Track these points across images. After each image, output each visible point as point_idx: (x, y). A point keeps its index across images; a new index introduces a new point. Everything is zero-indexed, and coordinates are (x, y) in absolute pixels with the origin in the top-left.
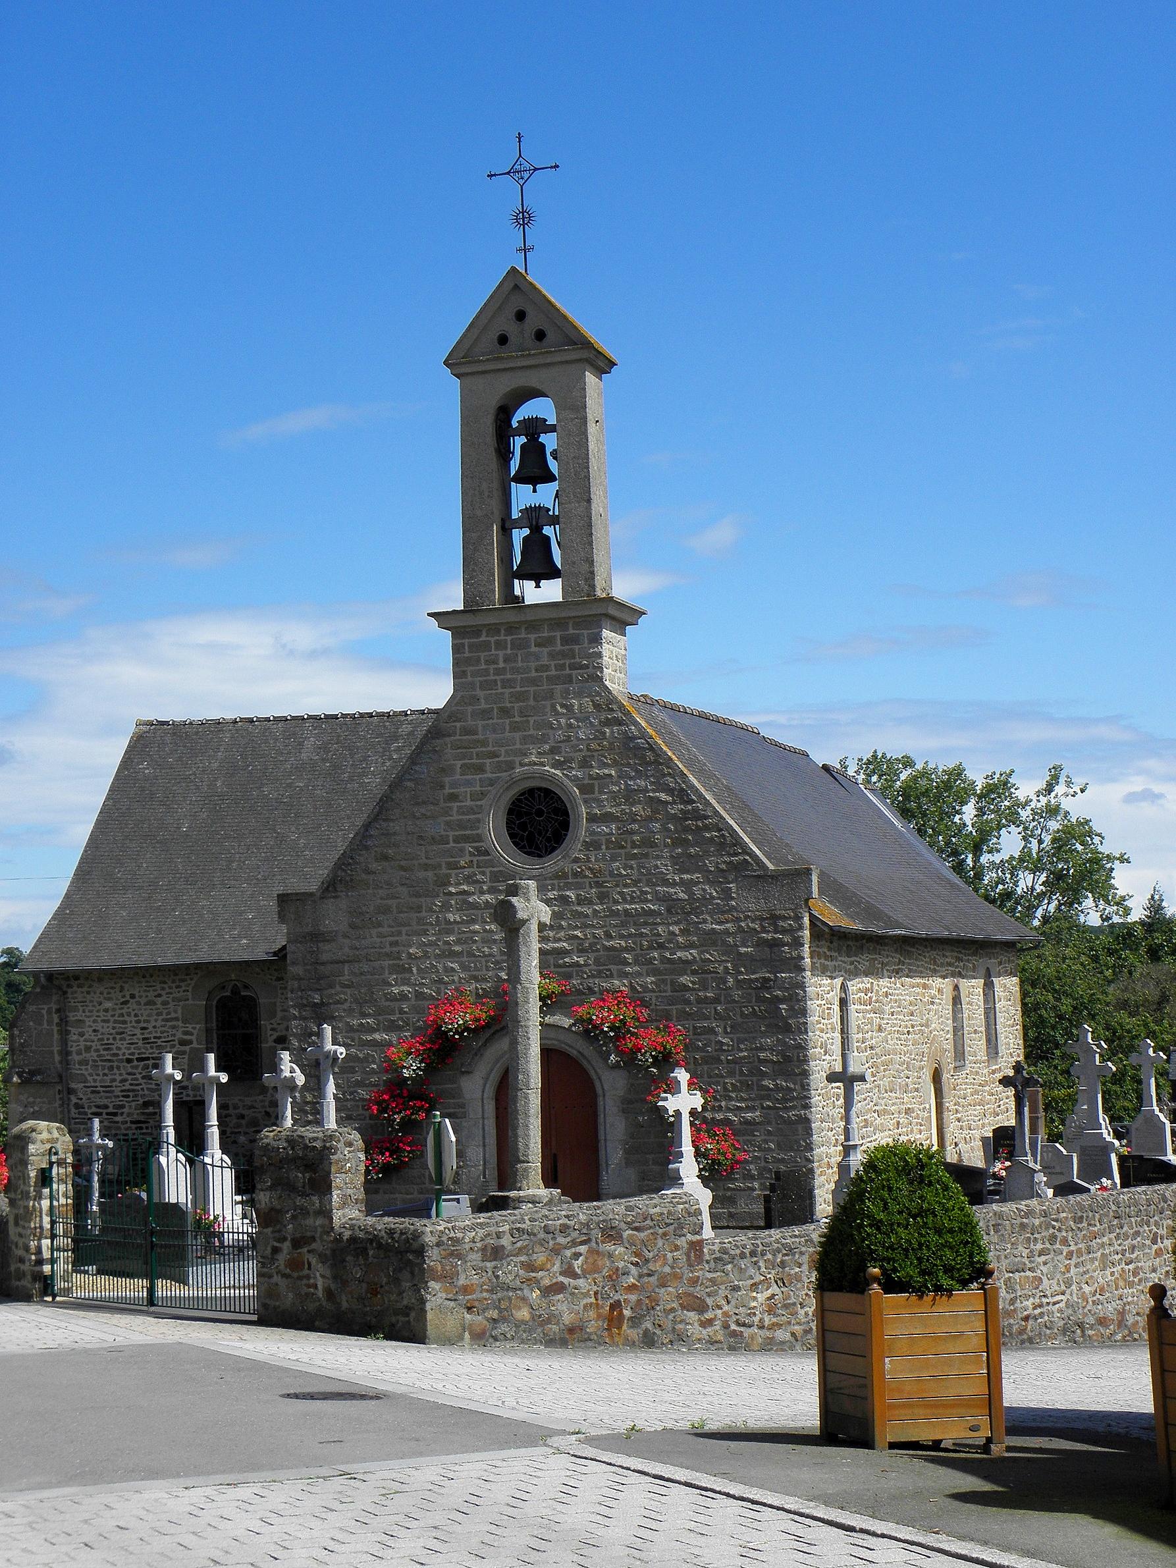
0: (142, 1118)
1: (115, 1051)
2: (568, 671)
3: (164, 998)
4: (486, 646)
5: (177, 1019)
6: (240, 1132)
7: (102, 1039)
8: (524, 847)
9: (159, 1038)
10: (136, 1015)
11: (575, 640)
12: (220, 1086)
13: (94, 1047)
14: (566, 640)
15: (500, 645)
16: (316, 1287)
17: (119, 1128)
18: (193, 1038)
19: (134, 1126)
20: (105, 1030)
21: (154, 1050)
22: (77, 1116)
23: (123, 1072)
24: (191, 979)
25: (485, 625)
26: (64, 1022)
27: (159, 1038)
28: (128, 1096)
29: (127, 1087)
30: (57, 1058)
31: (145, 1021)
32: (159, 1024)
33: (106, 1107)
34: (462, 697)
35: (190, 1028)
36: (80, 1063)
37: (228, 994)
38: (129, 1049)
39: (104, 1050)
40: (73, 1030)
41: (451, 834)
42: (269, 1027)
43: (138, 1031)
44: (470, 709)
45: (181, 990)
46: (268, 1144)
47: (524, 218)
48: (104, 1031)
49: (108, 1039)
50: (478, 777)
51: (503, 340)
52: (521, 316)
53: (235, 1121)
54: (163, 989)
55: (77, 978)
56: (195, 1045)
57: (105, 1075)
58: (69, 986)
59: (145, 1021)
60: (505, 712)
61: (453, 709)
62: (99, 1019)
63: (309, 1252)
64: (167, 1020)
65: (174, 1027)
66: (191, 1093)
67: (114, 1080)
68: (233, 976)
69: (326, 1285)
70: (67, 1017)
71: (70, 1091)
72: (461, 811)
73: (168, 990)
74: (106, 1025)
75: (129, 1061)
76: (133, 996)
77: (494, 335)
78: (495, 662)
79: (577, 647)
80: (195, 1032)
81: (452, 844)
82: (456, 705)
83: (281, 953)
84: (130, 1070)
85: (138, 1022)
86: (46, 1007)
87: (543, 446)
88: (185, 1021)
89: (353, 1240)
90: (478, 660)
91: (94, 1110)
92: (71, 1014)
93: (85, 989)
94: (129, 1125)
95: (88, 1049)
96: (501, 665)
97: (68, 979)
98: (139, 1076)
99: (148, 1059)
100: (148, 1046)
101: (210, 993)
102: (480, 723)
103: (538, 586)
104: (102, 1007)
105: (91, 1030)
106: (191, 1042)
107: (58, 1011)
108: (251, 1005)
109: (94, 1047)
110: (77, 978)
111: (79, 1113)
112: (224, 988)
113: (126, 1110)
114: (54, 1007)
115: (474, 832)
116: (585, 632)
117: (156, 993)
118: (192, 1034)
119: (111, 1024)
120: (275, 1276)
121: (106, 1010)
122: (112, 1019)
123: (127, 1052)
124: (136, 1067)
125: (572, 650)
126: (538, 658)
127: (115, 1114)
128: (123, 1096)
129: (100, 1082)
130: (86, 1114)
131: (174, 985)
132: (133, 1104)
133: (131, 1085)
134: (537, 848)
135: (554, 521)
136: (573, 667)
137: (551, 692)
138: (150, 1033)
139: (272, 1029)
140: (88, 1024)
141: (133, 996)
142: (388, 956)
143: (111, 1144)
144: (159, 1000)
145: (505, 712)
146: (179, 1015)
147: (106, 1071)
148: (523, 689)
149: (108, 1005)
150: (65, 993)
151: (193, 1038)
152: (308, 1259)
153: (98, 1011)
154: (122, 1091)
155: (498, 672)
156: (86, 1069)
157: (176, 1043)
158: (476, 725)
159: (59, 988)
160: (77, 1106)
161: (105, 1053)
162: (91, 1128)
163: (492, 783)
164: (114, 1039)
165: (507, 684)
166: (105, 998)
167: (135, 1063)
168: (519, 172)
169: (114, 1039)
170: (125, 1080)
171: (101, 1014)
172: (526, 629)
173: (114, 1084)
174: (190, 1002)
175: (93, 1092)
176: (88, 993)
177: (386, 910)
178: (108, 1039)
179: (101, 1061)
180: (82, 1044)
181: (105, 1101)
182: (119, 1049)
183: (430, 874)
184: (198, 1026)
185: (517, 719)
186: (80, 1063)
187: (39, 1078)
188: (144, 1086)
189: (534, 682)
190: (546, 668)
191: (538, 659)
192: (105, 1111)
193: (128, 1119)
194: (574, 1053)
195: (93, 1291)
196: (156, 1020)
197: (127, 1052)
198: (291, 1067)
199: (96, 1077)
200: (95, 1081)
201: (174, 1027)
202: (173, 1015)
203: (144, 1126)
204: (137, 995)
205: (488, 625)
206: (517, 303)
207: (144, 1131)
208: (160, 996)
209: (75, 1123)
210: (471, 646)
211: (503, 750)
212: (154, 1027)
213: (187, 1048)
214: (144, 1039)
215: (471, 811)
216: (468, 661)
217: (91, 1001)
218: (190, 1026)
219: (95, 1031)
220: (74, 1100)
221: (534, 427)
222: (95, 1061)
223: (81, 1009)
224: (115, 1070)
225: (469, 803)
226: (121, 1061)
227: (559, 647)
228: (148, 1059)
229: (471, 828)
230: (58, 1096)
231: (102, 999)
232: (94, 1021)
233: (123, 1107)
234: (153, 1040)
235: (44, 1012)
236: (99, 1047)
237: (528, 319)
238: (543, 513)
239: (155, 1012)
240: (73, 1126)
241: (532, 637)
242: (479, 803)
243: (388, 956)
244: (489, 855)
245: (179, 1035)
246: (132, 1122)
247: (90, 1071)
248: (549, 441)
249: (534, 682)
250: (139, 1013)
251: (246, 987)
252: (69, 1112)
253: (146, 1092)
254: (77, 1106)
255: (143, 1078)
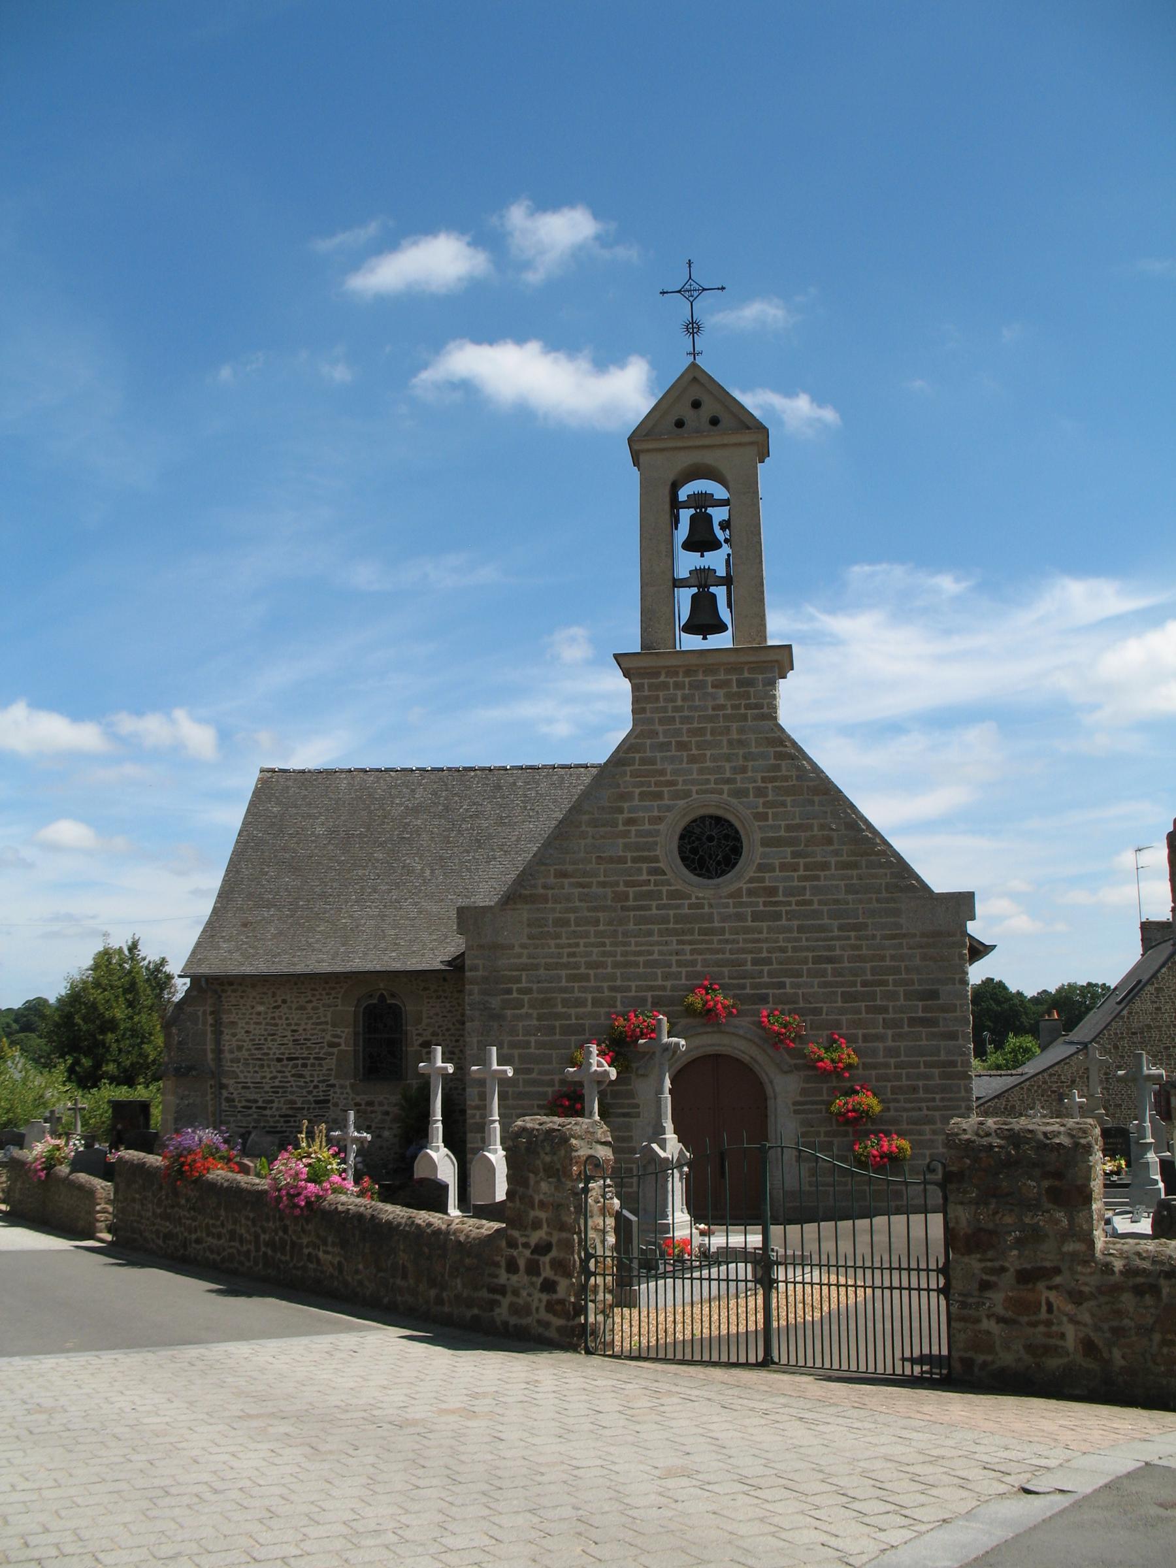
0: (290, 1112)
1: (265, 1051)
2: (743, 711)
3: (314, 1004)
4: (665, 686)
5: (326, 1023)
6: (384, 1128)
7: (254, 1040)
8: (695, 869)
9: (309, 1040)
10: (287, 1019)
11: (750, 683)
12: (504, 1081)
13: (246, 1047)
14: (740, 683)
15: (678, 686)
16: (1063, 1336)
17: (268, 1121)
18: (342, 1041)
19: (282, 1119)
20: (257, 1032)
21: (304, 1051)
22: (227, 1109)
23: (272, 1069)
24: (341, 987)
25: (664, 667)
26: (218, 1025)
27: (309, 1040)
28: (278, 1092)
29: (277, 1084)
30: (210, 1056)
31: (296, 1024)
32: (309, 1027)
33: (256, 1101)
34: (641, 730)
35: (339, 1031)
36: (232, 1061)
37: (375, 1001)
38: (280, 1049)
39: (256, 1049)
40: (226, 1031)
41: (629, 855)
42: (415, 1032)
43: (289, 1033)
44: (648, 742)
45: (331, 997)
46: (969, 1141)
47: (693, 328)
48: (256, 1032)
49: (260, 1040)
50: (655, 804)
51: (680, 424)
52: (696, 405)
53: (379, 1117)
54: (313, 995)
55: (231, 984)
56: (343, 1047)
57: (256, 1072)
58: (223, 991)
59: (296, 1024)
60: (682, 746)
61: (633, 741)
62: (252, 1022)
63: (1049, 1288)
64: (317, 1024)
65: (324, 1030)
66: (338, 1091)
67: (264, 1077)
68: (382, 986)
69: (1081, 1335)
70: (221, 1018)
71: (223, 1086)
72: (639, 834)
73: (318, 997)
74: (258, 1027)
75: (279, 1060)
76: (284, 1001)
77: (672, 419)
78: (673, 700)
79: (752, 690)
80: (344, 1035)
81: (629, 864)
82: (635, 738)
83: (457, 965)
84: (279, 1068)
85: (289, 1025)
86: (202, 1009)
87: (710, 517)
88: (334, 1025)
89: (1130, 1272)
90: (657, 699)
91: (244, 1104)
92: (225, 1016)
93: (239, 994)
94: (277, 1118)
95: (240, 1048)
96: (679, 703)
97: (222, 984)
98: (289, 1074)
99: (297, 1059)
100: (298, 1047)
101: (359, 1000)
102: (659, 755)
103: (705, 638)
104: (254, 1011)
105: (243, 1031)
106: (339, 1045)
107: (212, 1013)
108: (395, 1013)
109: (246, 1047)
110: (231, 984)
111: (230, 1106)
112: (371, 996)
113: (275, 1105)
114: (209, 1009)
115: (651, 854)
116: (760, 677)
117: (307, 999)
118: (340, 1037)
119: (263, 1027)
120: (985, 1321)
121: (259, 1014)
122: (264, 1022)
123: (278, 1052)
124: (286, 1066)
125: (748, 692)
126: (714, 699)
127: (265, 1108)
128: (273, 1092)
129: (251, 1078)
130: (236, 1107)
131: (324, 992)
132: (282, 1100)
133: (281, 1082)
134: (708, 870)
135: (721, 581)
136: (747, 707)
137: (728, 729)
138: (301, 1035)
139: (417, 1035)
140: (240, 1025)
141: (284, 1001)
142: (566, 966)
143: (369, 1137)
144: (310, 1006)
145: (682, 746)
146: (329, 1019)
147: (257, 1069)
148: (701, 726)
149: (261, 1008)
150: (220, 997)
151: (342, 1041)
152: (1047, 1299)
153: (251, 1014)
154: (272, 1087)
155: (676, 709)
156: (238, 1067)
157: (325, 1044)
158: (656, 756)
159: (216, 992)
160: (228, 1100)
161: (256, 1052)
162: (346, 1120)
163: (669, 808)
164: (266, 1040)
165: (686, 720)
166: (258, 1003)
167: (285, 1062)
168: (690, 291)
169: (266, 1040)
170: (275, 1078)
171: (254, 1016)
172: (704, 672)
173: (264, 1081)
174: (339, 1008)
175: (244, 1088)
176: (242, 997)
177: (565, 923)
178: (260, 1040)
179: (253, 1059)
180: (234, 1043)
181: (252, 1097)
182: (270, 1048)
183: (609, 890)
184: (346, 1030)
185: (694, 752)
186: (232, 1061)
187: (194, 1073)
188: (292, 1083)
189: (711, 719)
190: (722, 707)
191: (714, 699)
192: (254, 1105)
193: (277, 1113)
194: (746, 1059)
195: (674, 1322)
196: (306, 1024)
197: (278, 1052)
198: (598, 1061)
199: (246, 1074)
200: (246, 1077)
201: (324, 1030)
202: (323, 1019)
203: (292, 1119)
204: (289, 1000)
205: (668, 667)
206: (695, 393)
207: (292, 1124)
208: (310, 1001)
209: (226, 1116)
210: (651, 686)
211: (680, 779)
212: (305, 1030)
213: (335, 1050)
214: (294, 1041)
215: (649, 833)
216: (647, 699)
217: (244, 1005)
218: (339, 1030)
219: (247, 1032)
220: (225, 1094)
221: (701, 501)
222: (245, 1059)
223: (234, 1011)
224: (266, 1069)
225: (647, 827)
226: (272, 1060)
227: (735, 689)
228: (297, 1059)
229: (649, 850)
230: (209, 1091)
231: (254, 1004)
232: (247, 1023)
233: (272, 1102)
234: (302, 1042)
235: (200, 1013)
236: (250, 1047)
237: (703, 409)
238: (711, 573)
239: (305, 1016)
240: (223, 1118)
241: (710, 679)
242: (656, 827)
243: (566, 966)
244: (665, 874)
245: (328, 1038)
246: (281, 1116)
247: (242, 1068)
248: (719, 514)
249: (711, 719)
250: (290, 1016)
251: (393, 996)
252: (220, 1104)
253: (295, 1089)
254: (228, 1100)
255: (293, 1076)
